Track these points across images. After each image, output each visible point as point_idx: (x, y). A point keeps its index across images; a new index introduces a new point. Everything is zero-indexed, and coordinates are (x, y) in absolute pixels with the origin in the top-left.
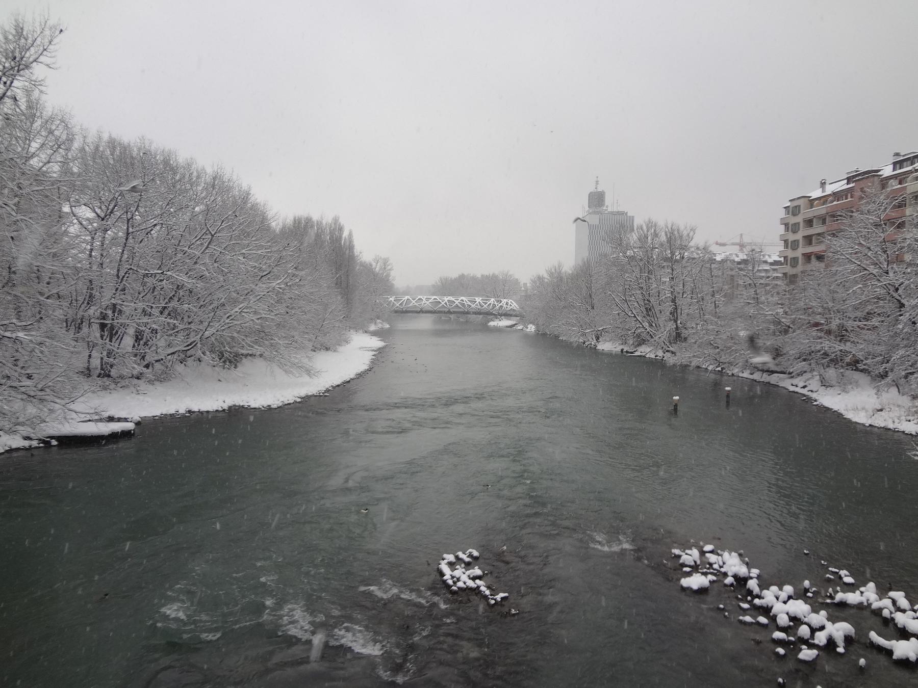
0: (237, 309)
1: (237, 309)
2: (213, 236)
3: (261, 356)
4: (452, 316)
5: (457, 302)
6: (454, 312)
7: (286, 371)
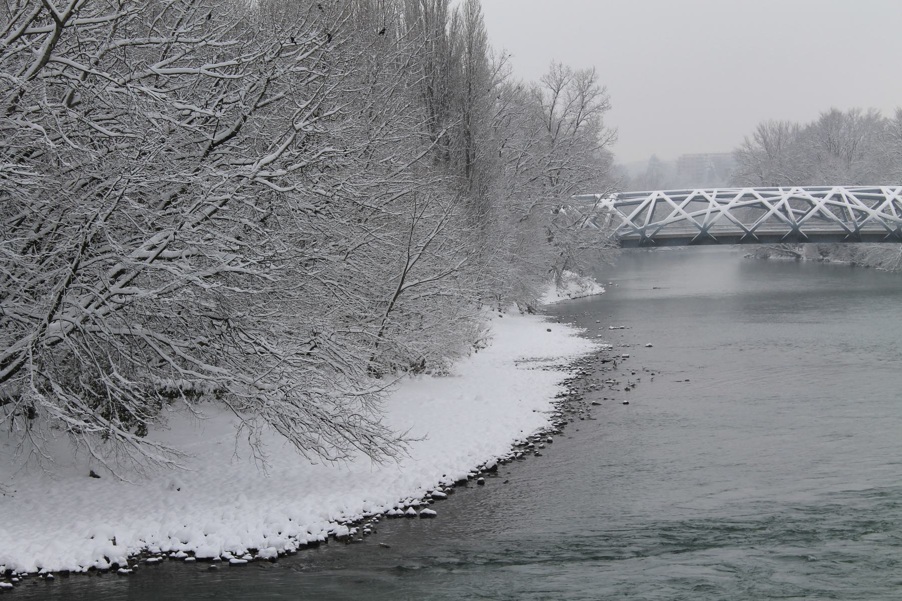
0: (142, 251)
1: (142, 251)
2: (61, 25)
3: (220, 394)
4: (804, 250)
5: (820, 203)
6: (812, 238)
7: (298, 443)
